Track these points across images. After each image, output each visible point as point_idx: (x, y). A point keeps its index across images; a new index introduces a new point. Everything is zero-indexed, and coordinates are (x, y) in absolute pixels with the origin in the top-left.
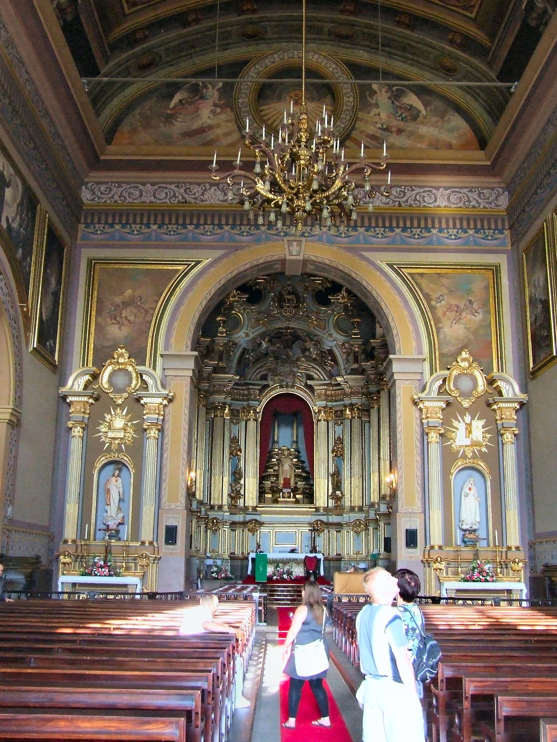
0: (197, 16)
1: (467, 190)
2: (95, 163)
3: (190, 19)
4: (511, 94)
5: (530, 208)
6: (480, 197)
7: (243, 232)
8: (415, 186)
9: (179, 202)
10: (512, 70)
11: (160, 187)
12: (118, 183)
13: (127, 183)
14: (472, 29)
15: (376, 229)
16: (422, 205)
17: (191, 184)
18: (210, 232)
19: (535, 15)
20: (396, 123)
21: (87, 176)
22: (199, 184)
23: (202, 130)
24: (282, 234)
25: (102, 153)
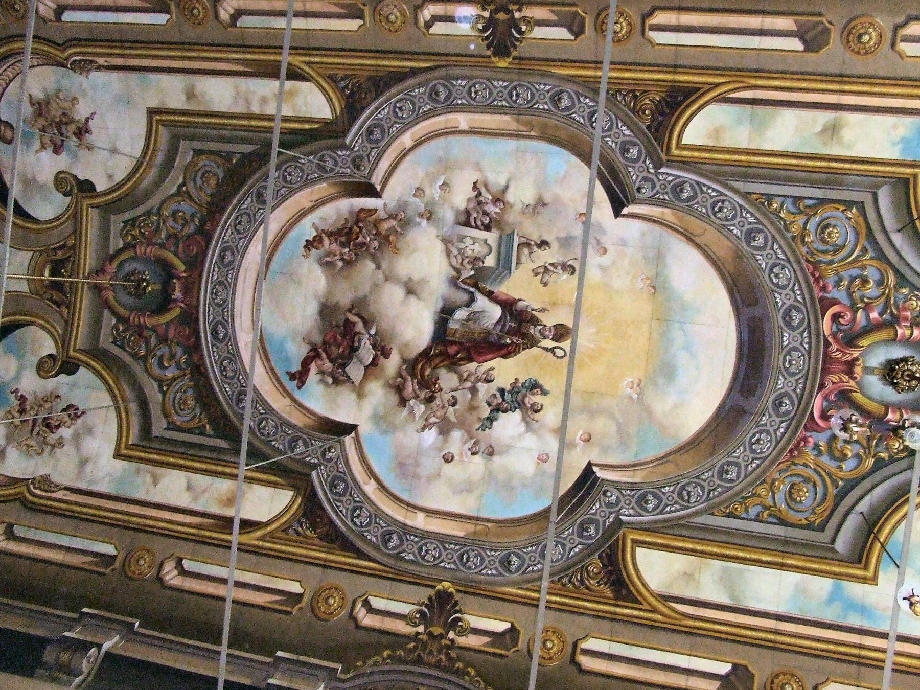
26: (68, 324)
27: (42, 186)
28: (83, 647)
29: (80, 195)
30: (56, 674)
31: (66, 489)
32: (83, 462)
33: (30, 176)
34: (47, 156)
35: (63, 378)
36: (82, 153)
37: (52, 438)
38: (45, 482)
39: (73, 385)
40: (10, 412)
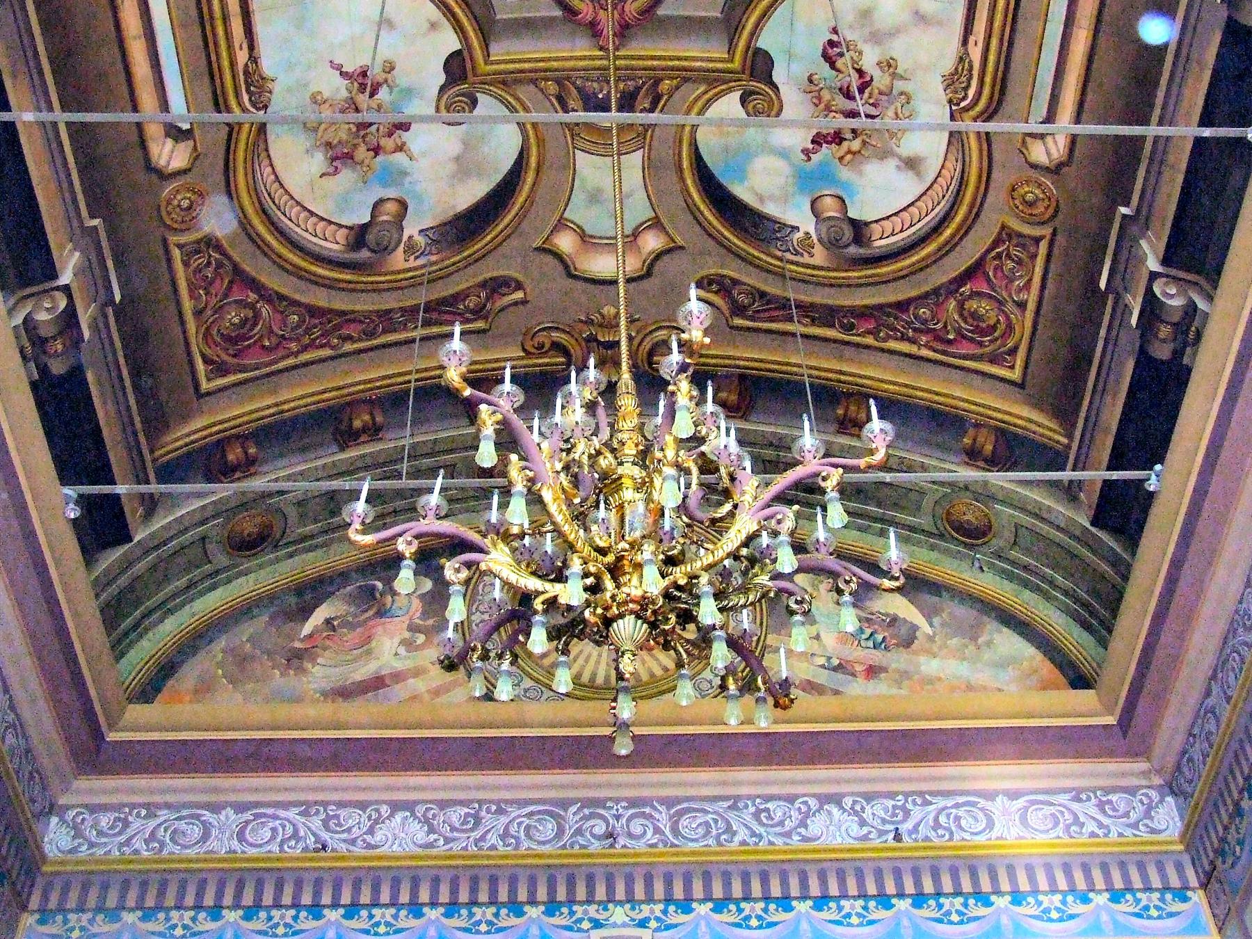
0: (373, 419)
1: (1067, 796)
2: (93, 751)
3: (357, 424)
4: (1151, 496)
5: (1230, 861)
6: (1104, 812)
7: (479, 923)
8: (932, 793)
9: (306, 849)
10: (1146, 436)
11: (257, 816)
12: (147, 806)
13: (168, 806)
14: (1016, 409)
15: (843, 902)
16: (956, 837)
17: (341, 804)
18: (387, 924)
19: (1164, 331)
20: (862, 655)
21: (66, 790)
22: (363, 806)
23: (377, 683)
24: (586, 925)
25: (112, 727)
26: (686, 76)
27: (466, 144)
28: (1152, 305)
29: (471, 78)
30: (1191, 335)
31: (965, 42)
32: (920, 18)
33: (451, 167)
34: (416, 139)
35: (778, 76)
36: (402, 78)
37: (880, 80)
38: (954, 81)
39: (790, 56)
40: (841, 159)
